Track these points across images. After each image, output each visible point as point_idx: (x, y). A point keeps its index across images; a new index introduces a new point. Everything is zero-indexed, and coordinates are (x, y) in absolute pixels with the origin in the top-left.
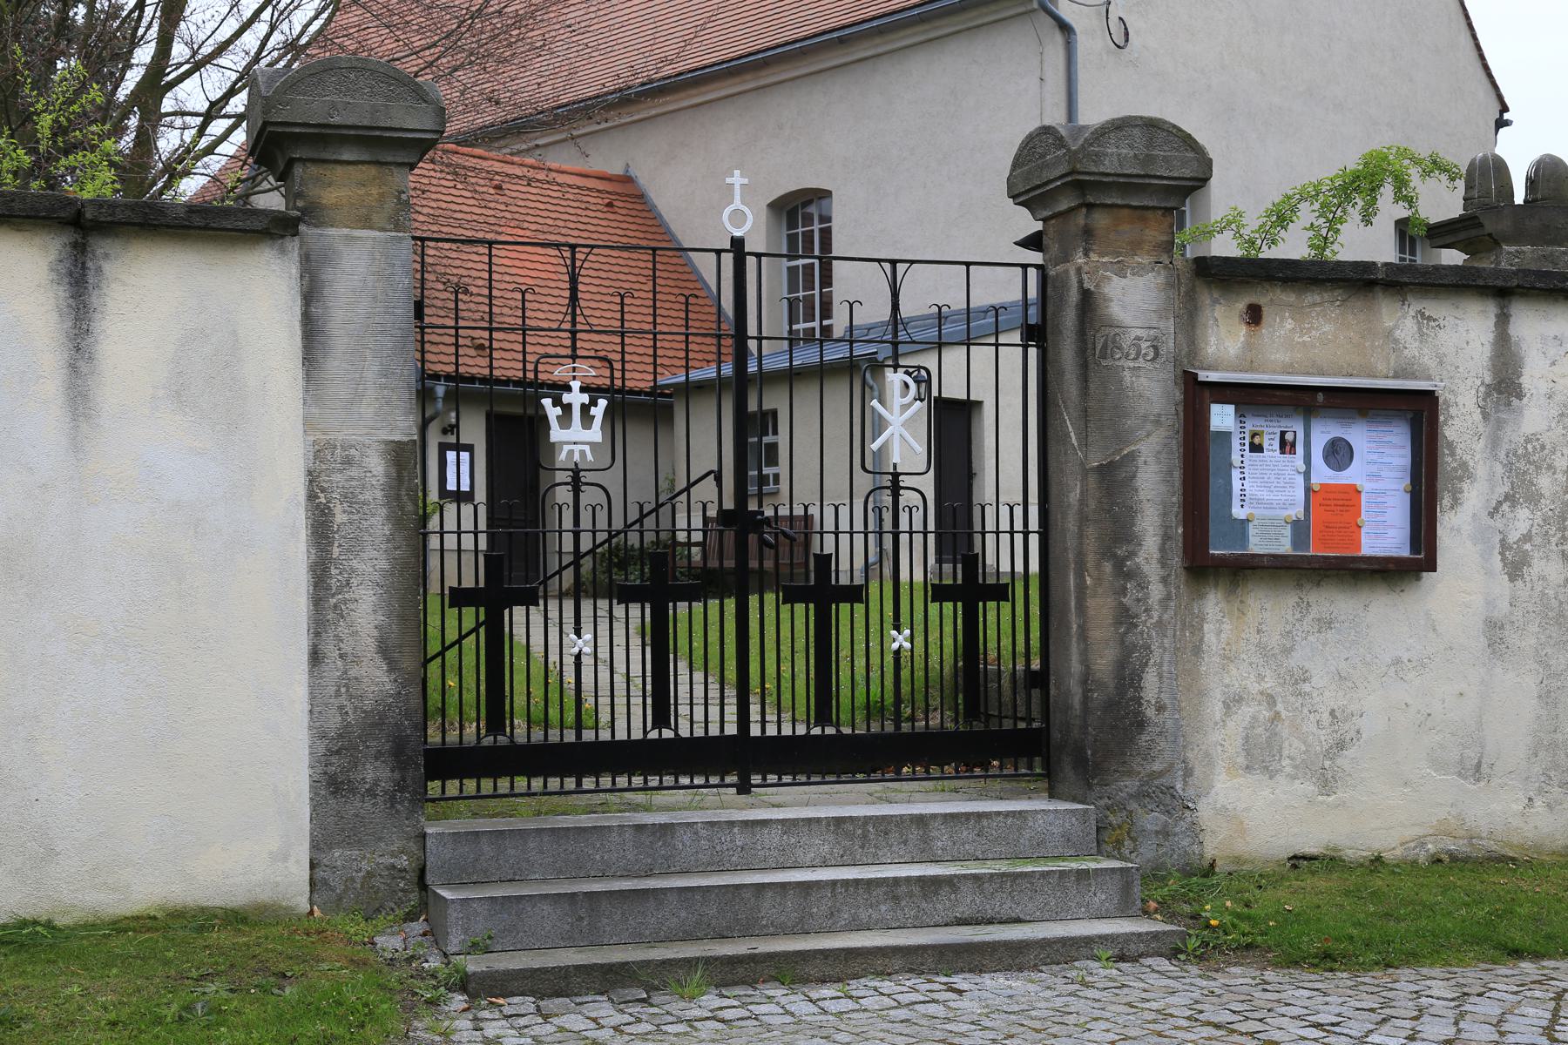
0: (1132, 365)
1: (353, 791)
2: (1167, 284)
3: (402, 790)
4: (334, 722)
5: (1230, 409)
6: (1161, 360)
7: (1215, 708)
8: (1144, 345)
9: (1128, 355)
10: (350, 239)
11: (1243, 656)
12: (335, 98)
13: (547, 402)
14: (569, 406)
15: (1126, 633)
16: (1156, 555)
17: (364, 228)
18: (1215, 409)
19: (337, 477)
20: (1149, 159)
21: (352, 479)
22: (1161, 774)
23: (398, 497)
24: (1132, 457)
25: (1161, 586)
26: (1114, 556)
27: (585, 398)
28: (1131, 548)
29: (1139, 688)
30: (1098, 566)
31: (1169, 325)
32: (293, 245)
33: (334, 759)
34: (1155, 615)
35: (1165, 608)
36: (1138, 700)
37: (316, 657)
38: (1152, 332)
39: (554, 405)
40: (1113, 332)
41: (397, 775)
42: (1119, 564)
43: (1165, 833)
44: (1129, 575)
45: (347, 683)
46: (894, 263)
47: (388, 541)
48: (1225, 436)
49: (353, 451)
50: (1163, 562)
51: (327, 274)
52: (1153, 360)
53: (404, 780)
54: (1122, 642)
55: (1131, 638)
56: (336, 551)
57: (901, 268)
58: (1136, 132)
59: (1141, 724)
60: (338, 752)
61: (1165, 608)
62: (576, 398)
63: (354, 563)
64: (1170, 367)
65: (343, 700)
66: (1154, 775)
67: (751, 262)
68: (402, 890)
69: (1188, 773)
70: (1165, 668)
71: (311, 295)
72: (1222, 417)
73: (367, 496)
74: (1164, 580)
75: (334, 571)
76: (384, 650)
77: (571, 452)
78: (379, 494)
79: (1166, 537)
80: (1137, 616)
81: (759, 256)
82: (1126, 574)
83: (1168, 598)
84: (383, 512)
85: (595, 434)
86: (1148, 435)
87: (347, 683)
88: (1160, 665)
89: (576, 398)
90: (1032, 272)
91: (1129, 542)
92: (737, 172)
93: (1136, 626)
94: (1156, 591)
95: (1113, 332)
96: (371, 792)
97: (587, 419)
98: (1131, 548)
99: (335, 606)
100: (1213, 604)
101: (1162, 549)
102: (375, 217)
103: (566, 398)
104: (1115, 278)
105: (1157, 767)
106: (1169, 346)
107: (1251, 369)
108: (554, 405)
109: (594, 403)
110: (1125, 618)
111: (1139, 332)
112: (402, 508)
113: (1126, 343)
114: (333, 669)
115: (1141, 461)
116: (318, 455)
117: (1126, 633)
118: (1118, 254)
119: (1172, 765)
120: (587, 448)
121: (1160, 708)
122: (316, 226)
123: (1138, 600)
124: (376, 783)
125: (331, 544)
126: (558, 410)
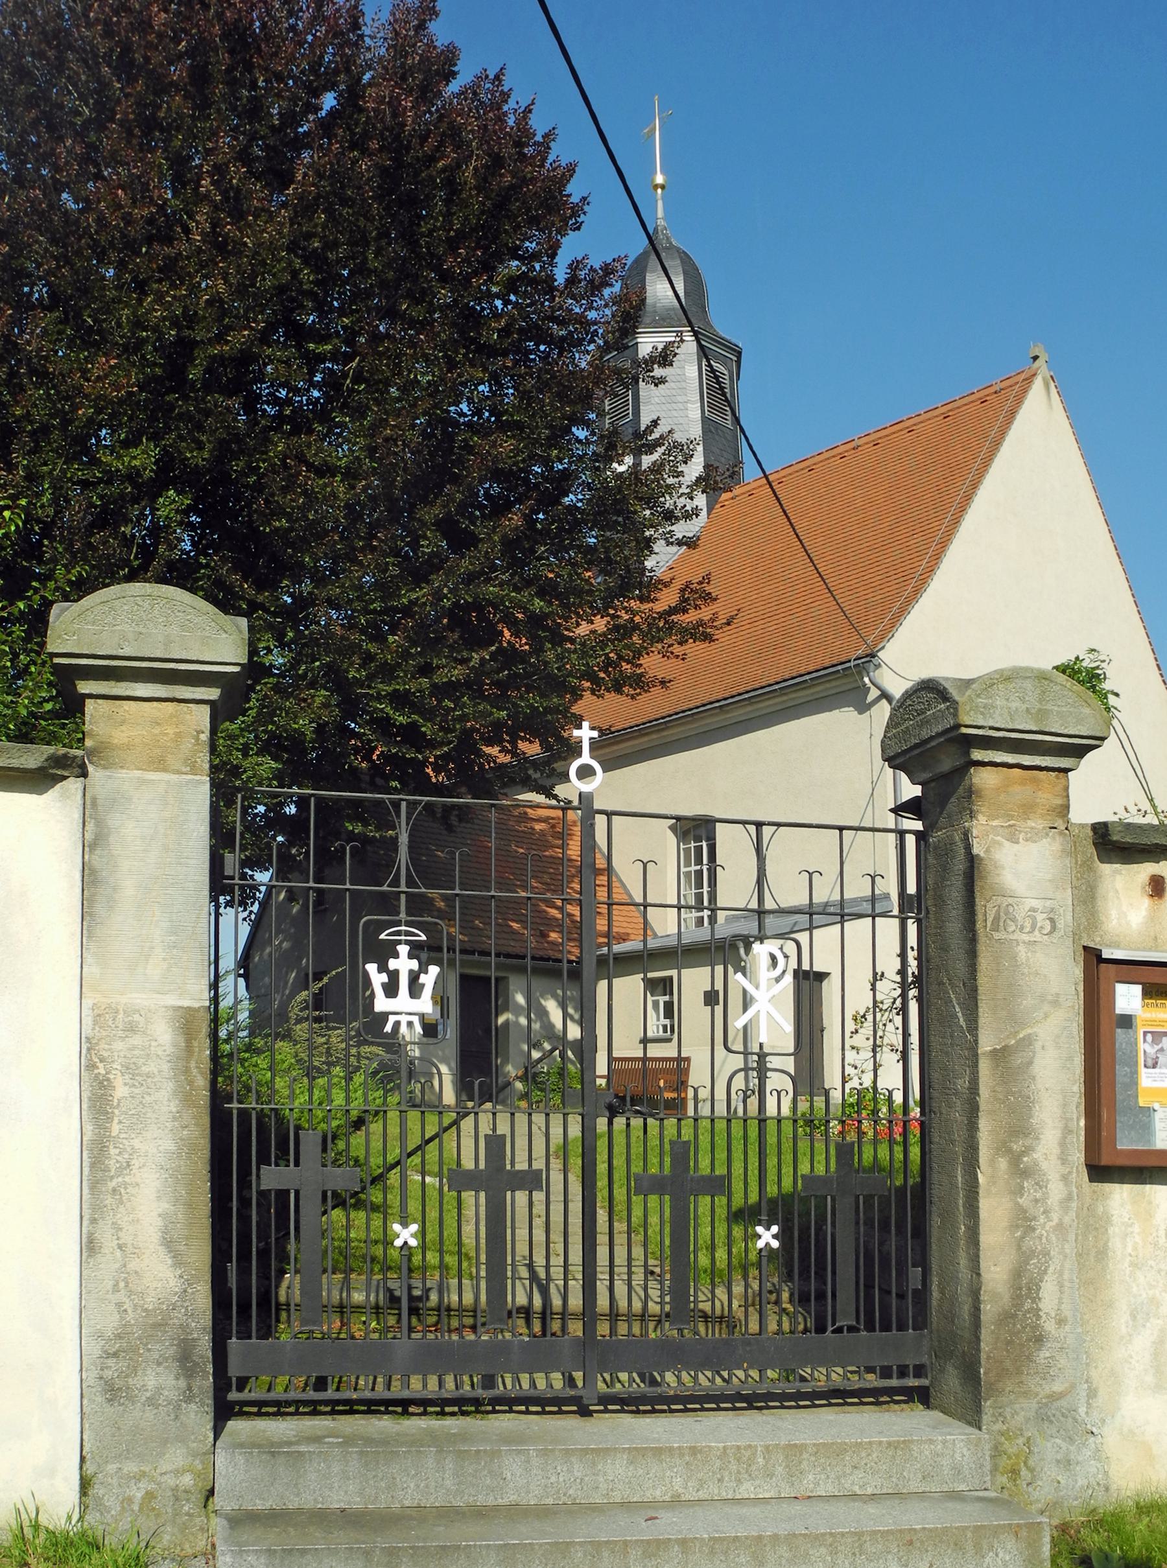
0: (1026, 937)
1: (131, 1399)
2: (1063, 851)
3: (189, 1399)
4: (110, 1322)
5: (1137, 989)
6: (1056, 935)
7: (1121, 1320)
8: (1040, 917)
9: (1022, 928)
10: (143, 782)
11: (1151, 1262)
12: (126, 627)
13: (372, 968)
14: (396, 972)
15: (1023, 1237)
16: (1056, 1150)
17: (157, 770)
18: (1121, 989)
19: (119, 1045)
20: (1042, 714)
21: (134, 1048)
22: (1061, 1395)
23: (187, 1071)
24: (1028, 1041)
25: (1061, 1185)
26: (1010, 1151)
27: (414, 965)
28: (1028, 1142)
29: (1036, 1299)
30: (992, 1162)
31: (1066, 897)
32: (73, 785)
33: (111, 1362)
34: (1055, 1217)
35: (1066, 1209)
36: (1037, 1312)
37: (90, 1247)
38: (1048, 903)
39: (380, 971)
40: (1005, 901)
41: (182, 1383)
42: (1016, 1160)
43: (1066, 1463)
44: (1025, 1173)
45: (125, 1280)
46: (759, 825)
47: (175, 1119)
48: (1126, 1021)
49: (136, 1017)
50: (1063, 1160)
51: (114, 820)
52: (1051, 933)
53: (190, 1388)
54: (1019, 1247)
55: (1029, 1243)
56: (115, 1128)
57: (767, 831)
58: (1028, 684)
59: (1039, 1340)
60: (115, 1355)
61: (1066, 1209)
62: (403, 963)
63: (136, 1143)
64: (1069, 942)
65: (121, 1296)
66: (1054, 1397)
67: (600, 821)
68: (188, 1514)
69: (1092, 1393)
70: (1066, 1277)
71: (94, 842)
72: (1128, 998)
73: (152, 1067)
74: (1065, 1178)
75: (113, 1151)
76: (168, 1243)
77: (397, 1024)
78: (166, 1067)
79: (1067, 1131)
80: (1035, 1218)
81: (609, 814)
82: (1022, 1171)
83: (1069, 1198)
84: (170, 1086)
85: (425, 1004)
86: (1046, 1016)
87: (125, 1280)
88: (1061, 1273)
89: (403, 963)
90: (910, 840)
91: (1026, 1135)
92: (775, 1244)
93: (1034, 1229)
94: (1056, 1191)
95: (1005, 901)
96: (151, 1402)
97: (415, 990)
98: (1028, 1142)
99: (114, 1190)
100: (1120, 1195)
101: (1063, 1144)
102: (170, 760)
103: (393, 964)
104: (1007, 844)
105: (1057, 1387)
106: (1066, 920)
107: (1156, 949)
108: (380, 971)
109: (423, 969)
110: (1023, 1222)
111: (1035, 903)
112: (191, 1083)
113: (1020, 913)
114: (108, 1263)
115: (1038, 1045)
116: (97, 1019)
117: (1023, 1237)
118: (1012, 817)
119: (1073, 1386)
120: (415, 1020)
121: (1061, 1322)
122: (105, 768)
123: (1036, 1201)
124: (159, 1389)
125: (110, 1120)
126: (384, 977)
